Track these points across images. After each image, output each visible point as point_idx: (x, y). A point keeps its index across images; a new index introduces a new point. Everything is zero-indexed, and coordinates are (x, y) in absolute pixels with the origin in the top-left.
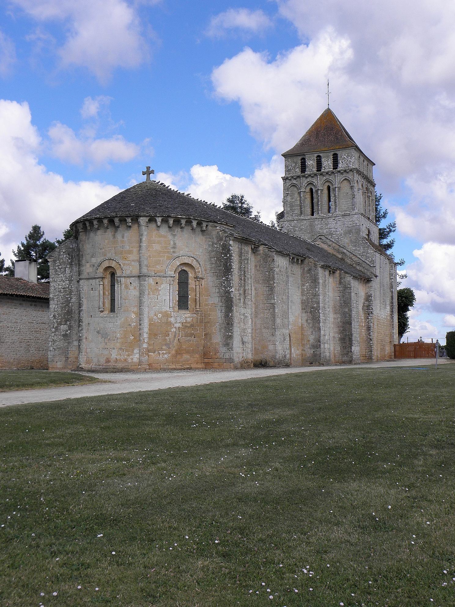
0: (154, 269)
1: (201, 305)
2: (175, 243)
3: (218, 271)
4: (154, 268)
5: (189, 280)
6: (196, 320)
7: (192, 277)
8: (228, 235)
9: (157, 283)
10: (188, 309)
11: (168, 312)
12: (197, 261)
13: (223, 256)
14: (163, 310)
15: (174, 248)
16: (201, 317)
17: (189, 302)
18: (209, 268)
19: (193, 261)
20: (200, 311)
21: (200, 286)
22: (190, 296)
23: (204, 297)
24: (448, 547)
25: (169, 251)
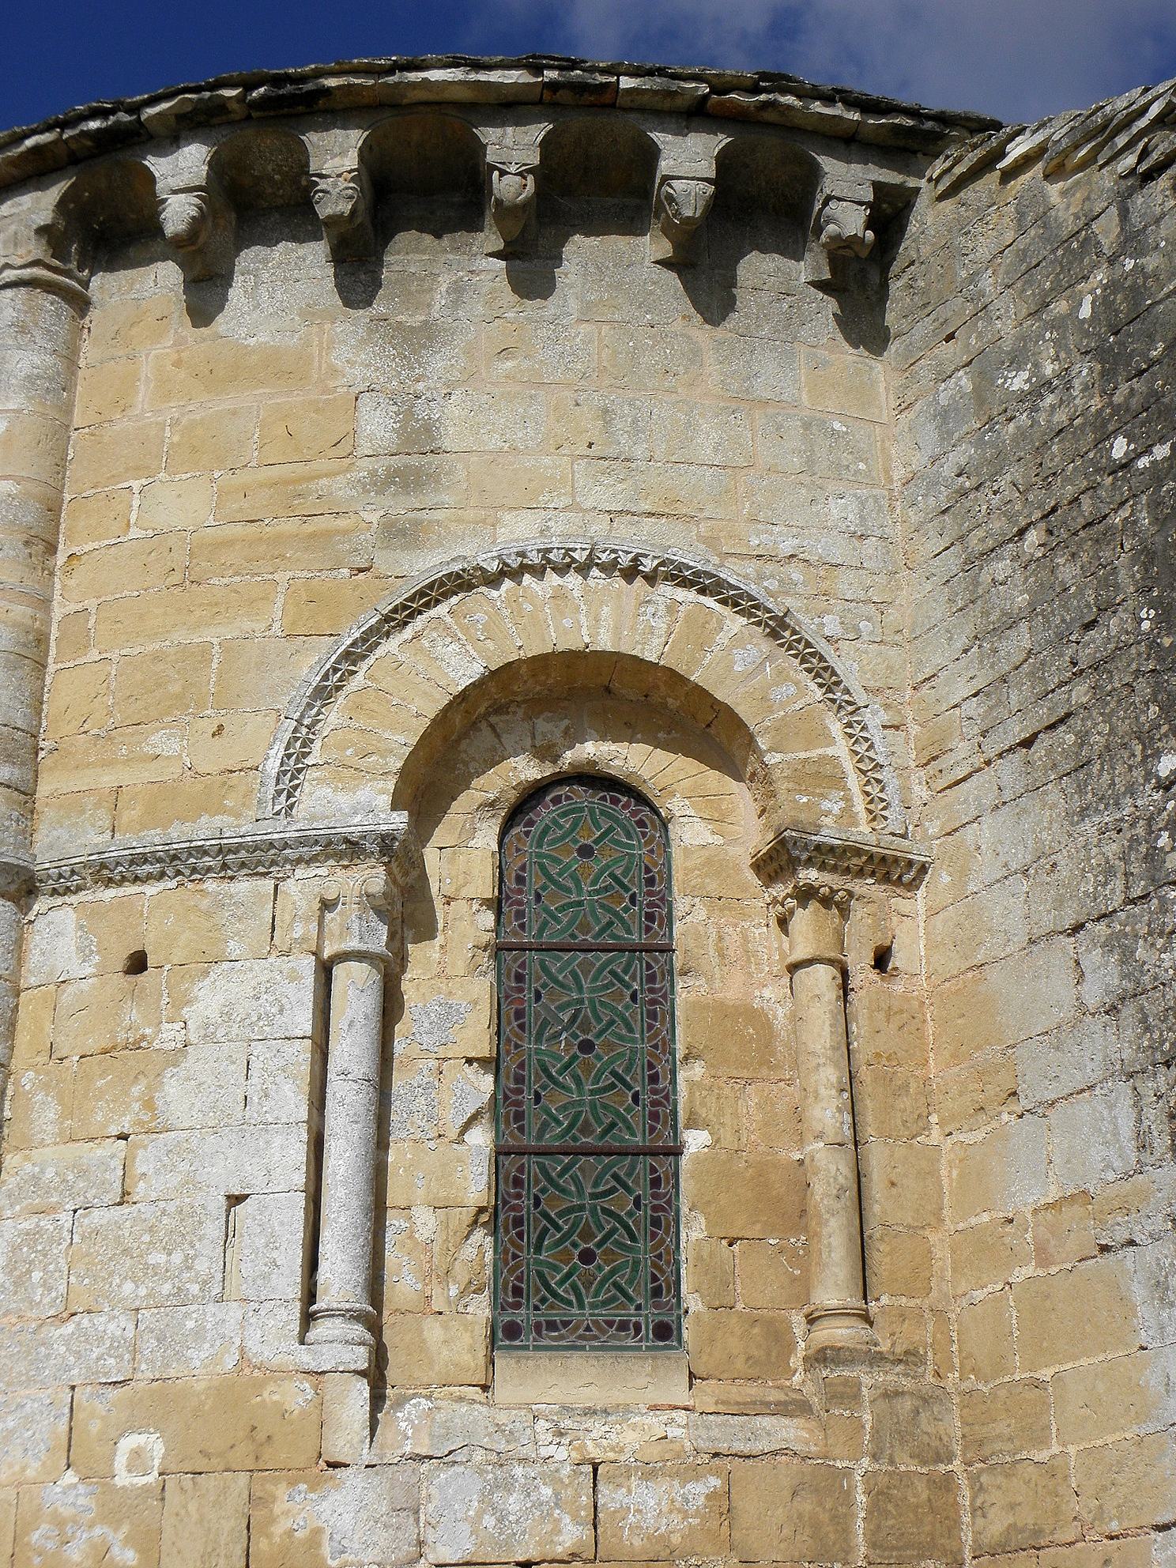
0: (108, 780)
1: (880, 1258)
2: (429, 429)
3: (1080, 693)
4: (109, 764)
5: (681, 905)
6: (806, 1505)
7: (715, 864)
8: (1144, 154)
9: (137, 964)
10: (665, 1332)
11: (272, 1395)
12: (777, 627)
13: (1120, 448)
14: (198, 1356)
15: (404, 480)
16: (907, 1465)
17: (693, 1232)
18: (972, 707)
19: (700, 633)
20: (876, 1359)
21: (862, 972)
22: (695, 1141)
23: (936, 1135)
24: (986, 826)
25: (342, 523)
